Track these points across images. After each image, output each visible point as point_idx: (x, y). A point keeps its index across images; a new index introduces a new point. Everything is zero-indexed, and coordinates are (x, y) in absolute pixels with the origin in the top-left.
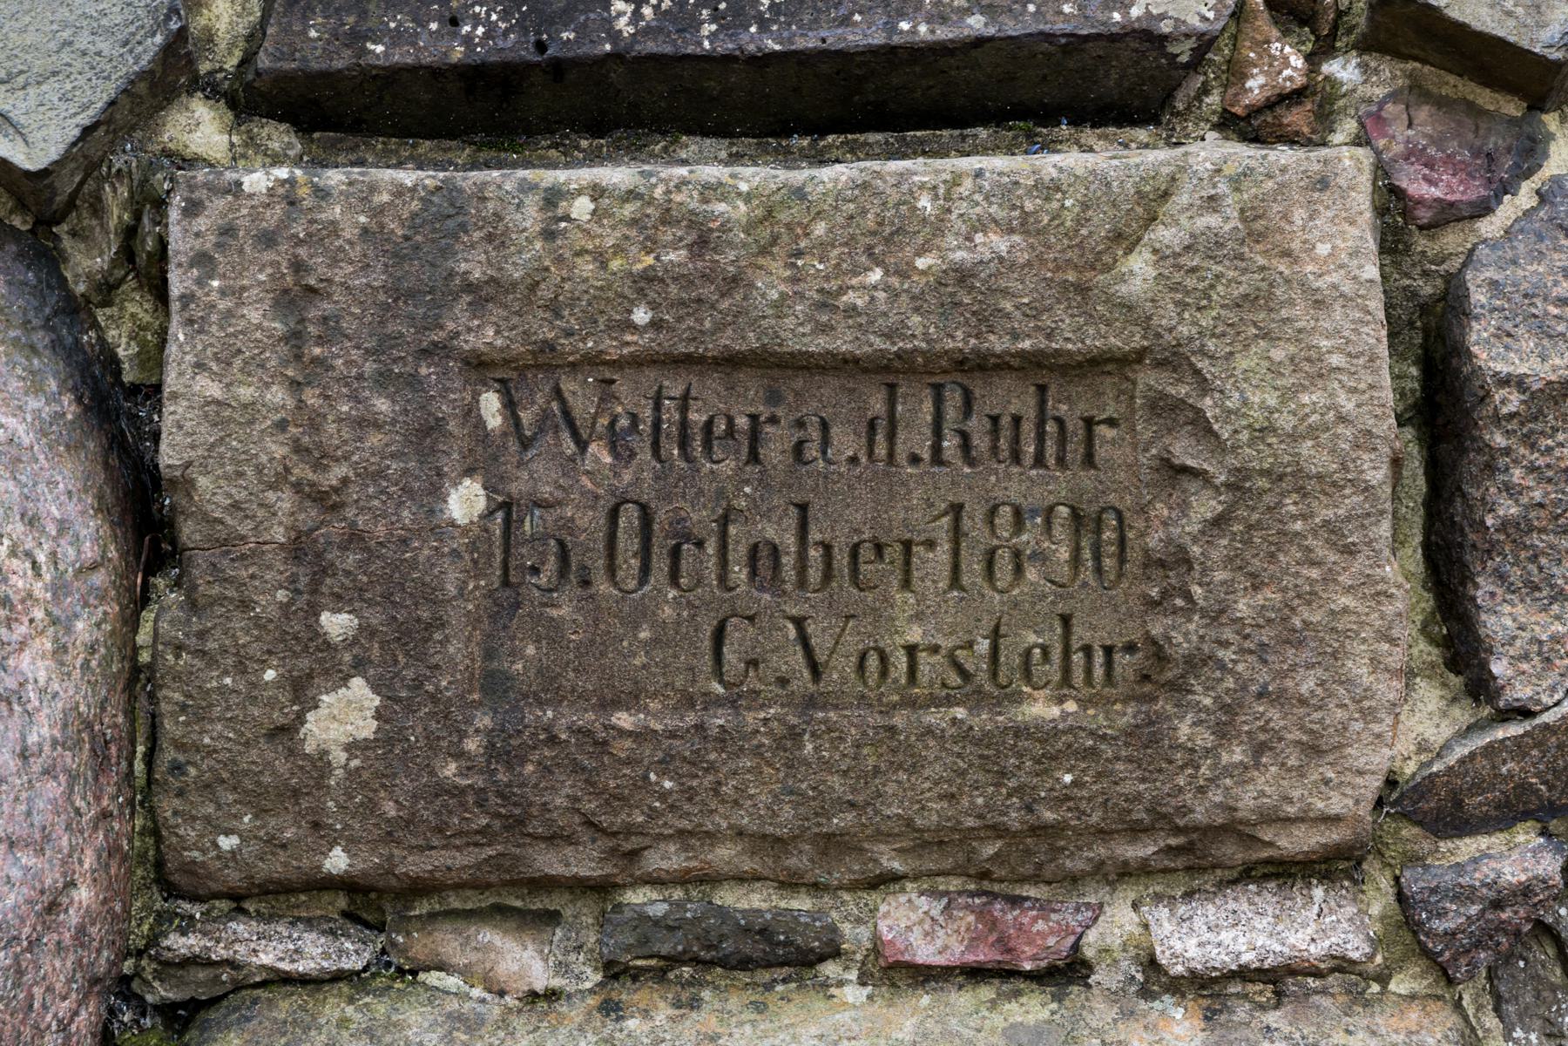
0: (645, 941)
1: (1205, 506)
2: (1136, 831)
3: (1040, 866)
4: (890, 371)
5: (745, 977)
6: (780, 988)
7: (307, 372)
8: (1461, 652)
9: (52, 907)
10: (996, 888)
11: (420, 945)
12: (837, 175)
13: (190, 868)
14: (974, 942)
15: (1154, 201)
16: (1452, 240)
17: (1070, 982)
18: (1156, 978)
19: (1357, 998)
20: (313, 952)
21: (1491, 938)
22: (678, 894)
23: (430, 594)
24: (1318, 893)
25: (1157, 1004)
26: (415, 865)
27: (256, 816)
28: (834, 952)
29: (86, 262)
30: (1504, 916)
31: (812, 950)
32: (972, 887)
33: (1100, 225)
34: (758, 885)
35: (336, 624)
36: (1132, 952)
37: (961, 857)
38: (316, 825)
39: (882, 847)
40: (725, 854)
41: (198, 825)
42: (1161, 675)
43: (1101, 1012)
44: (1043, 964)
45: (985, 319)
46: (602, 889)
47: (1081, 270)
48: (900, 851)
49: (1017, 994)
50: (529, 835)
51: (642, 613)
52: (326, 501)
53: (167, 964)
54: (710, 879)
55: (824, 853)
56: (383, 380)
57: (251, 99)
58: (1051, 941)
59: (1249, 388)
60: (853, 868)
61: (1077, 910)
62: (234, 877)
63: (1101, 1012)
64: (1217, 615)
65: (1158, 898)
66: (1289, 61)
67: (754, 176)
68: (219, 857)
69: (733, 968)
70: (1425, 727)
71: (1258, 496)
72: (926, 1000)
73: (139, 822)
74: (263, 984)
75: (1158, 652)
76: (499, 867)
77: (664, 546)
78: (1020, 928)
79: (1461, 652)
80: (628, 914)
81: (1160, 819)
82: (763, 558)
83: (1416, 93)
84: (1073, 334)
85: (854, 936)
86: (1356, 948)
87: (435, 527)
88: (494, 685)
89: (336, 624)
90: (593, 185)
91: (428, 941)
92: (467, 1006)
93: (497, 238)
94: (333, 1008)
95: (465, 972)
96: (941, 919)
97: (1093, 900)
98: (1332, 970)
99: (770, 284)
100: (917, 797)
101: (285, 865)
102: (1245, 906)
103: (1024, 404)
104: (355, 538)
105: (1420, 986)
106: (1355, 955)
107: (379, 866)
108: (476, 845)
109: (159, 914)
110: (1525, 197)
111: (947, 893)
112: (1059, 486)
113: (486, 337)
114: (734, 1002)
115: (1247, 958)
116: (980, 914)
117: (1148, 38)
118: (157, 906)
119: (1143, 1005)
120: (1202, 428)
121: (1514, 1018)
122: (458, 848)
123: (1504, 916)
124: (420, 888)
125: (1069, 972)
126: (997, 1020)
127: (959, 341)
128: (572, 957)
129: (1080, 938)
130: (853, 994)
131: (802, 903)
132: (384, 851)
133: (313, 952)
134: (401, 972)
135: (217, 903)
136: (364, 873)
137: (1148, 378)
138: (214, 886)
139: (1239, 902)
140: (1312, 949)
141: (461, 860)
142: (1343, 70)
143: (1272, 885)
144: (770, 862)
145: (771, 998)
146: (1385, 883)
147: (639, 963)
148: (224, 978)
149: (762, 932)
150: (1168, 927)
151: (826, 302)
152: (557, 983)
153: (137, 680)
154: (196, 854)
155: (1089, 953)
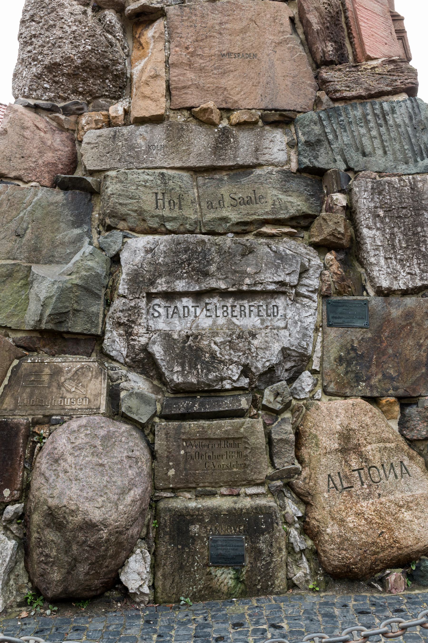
1: (249, 451)
2: (244, 481)
4: (220, 439)
7: (168, 441)
8: (273, 464)
11: (178, 494)
12: (215, 422)
15: (243, 424)
16: (270, 427)
18: (246, 495)
19: (265, 497)
20: (169, 495)
23: (179, 461)
26: (178, 486)
28: (217, 494)
29: (147, 432)
33: (239, 426)
35: (171, 464)
40: (207, 484)
42: (246, 466)
43: (241, 498)
45: (229, 434)
46: (195, 488)
47: (237, 430)
51: (199, 462)
52: (170, 452)
54: (205, 487)
56: (175, 441)
57: (163, 417)
59: (252, 440)
60: (218, 485)
63: (241, 498)
64: (250, 461)
66: (255, 411)
67: (207, 422)
70: (270, 471)
71: (253, 450)
75: (245, 464)
77: (200, 456)
79: (273, 464)
81: (246, 480)
82: (209, 457)
83: (266, 414)
84: (237, 436)
85: (218, 492)
87: (180, 454)
88: (185, 469)
89: (171, 464)
90: (193, 424)
93: (185, 428)
94: (171, 500)
99: (209, 432)
100: (224, 478)
103: (232, 442)
104: (172, 456)
110: (277, 423)
112: (235, 450)
113: (184, 437)
117: (242, 410)
120: (248, 444)
124: (179, 488)
125: (238, 495)
127: (226, 436)
133: (169, 495)
137: (243, 439)
139: (254, 488)
141: (182, 485)
142: (260, 412)
151: (214, 433)
153: (153, 470)
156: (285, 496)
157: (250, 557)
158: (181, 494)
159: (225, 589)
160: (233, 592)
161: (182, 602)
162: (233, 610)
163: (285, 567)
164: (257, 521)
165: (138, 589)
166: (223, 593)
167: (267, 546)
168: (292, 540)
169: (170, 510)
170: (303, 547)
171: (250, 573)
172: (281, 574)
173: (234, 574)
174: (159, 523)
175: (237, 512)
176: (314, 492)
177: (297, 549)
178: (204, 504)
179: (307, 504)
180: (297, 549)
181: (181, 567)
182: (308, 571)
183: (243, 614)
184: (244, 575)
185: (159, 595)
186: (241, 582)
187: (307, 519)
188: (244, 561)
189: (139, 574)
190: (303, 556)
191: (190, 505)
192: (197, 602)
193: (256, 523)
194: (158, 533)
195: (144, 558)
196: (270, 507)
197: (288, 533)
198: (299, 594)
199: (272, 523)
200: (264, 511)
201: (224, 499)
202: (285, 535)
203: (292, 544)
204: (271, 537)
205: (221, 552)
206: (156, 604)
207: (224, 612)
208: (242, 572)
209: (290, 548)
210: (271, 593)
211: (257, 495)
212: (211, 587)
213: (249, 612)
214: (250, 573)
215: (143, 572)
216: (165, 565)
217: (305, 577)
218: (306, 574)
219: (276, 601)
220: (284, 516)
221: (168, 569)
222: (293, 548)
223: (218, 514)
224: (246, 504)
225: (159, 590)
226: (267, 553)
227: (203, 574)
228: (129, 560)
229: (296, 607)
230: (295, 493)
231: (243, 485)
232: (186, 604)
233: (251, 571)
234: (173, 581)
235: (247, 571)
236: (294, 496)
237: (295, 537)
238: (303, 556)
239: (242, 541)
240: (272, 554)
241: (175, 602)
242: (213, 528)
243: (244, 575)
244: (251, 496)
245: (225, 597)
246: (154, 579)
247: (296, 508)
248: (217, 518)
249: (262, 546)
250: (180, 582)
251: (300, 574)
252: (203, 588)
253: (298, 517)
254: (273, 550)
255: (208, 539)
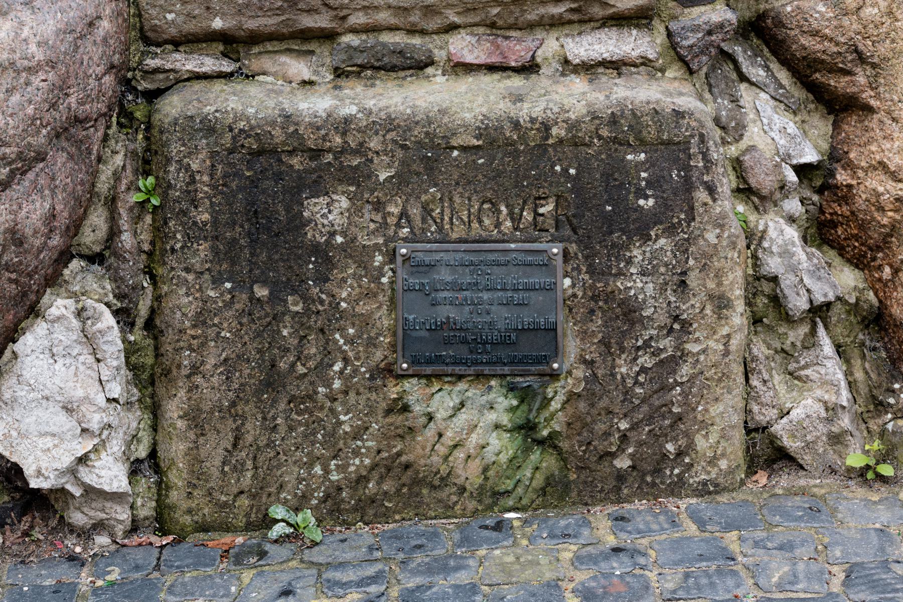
0: (350, 58)
3: (517, 19)
5: (394, 75)
6: (409, 79)
9: (91, 24)
10: (499, 32)
11: (255, 64)
13: (154, 29)
14: (490, 54)
17: (531, 73)
18: (568, 67)
21: (707, 49)
22: (364, 37)
24: (634, 32)
25: (568, 78)
26: (251, 24)
27: (182, 5)
28: (431, 63)
30: (713, 38)
31: (422, 61)
32: (489, 32)
34: (398, 32)
36: (557, 58)
37: (483, 16)
38: (208, 8)
39: (450, 11)
40: (383, 17)
41: (157, 9)
44: (520, 64)
46: (328, 36)
48: (458, 13)
49: (509, 77)
50: (299, 10)
53: (146, 72)
55: (425, 15)
58: (523, 54)
60: (433, 24)
61: (533, 40)
62: (173, 31)
65: (567, 35)
68: (167, 23)
69: (389, 71)
72: (471, 79)
73: (132, 11)
74: (188, 80)
76: (287, 25)
78: (509, 48)
80: (343, 45)
85: (440, 55)
86: (651, 55)
91: (259, 62)
92: (275, 87)
94: (218, 86)
95: (275, 75)
96: (476, 45)
97: (539, 37)
98: (643, 64)
101: (195, 26)
102: (604, 36)
105: (678, 74)
106: (651, 57)
107: (236, 25)
108: (277, 15)
109: (142, 53)
111: (478, 34)
114: (389, 84)
115: (605, 56)
116: (492, 43)
118: (142, 49)
119: (562, 79)
121: (717, 94)
122: (269, 16)
123: (713, 38)
124: (255, 39)
125: (530, 68)
126: (501, 85)
128: (320, 69)
129: (535, 53)
130: (440, 79)
131: (416, 41)
132: (238, 19)
133: (209, 64)
134: (247, 77)
135: (167, 46)
136: (229, 29)
138: (165, 36)
139: (603, 34)
140: (633, 53)
141: (267, 23)
143: (615, 28)
144: (402, 19)
145: (405, 83)
146: (662, 29)
147: (349, 69)
148: (171, 77)
149: (400, 52)
150: (571, 45)
152: (314, 78)
154: (156, 21)
155: (539, 60)
156: (743, 78)
157: (584, 335)
158: (266, 63)
159: (470, 474)
160: (509, 484)
161: (279, 529)
162: (504, 568)
163: (741, 379)
164: (616, 180)
165: (72, 472)
166: (463, 489)
167: (663, 289)
168: (773, 265)
169: (209, 128)
170: (822, 293)
171: (582, 406)
172: (723, 411)
173: (512, 410)
174: (163, 187)
175: (523, 138)
176: (884, 49)
177: (798, 303)
178: (370, 104)
179: (840, 107)
180: (798, 303)
181: (272, 381)
182: (845, 397)
183: (554, 585)
184: (555, 417)
185: (174, 496)
186: (541, 442)
187: (842, 177)
188: (556, 352)
189: (68, 409)
190: (821, 331)
191: (303, 106)
192: (348, 525)
193: (610, 193)
194: (159, 232)
195: (89, 340)
196: (679, 114)
197: (754, 239)
198: (803, 492)
199: (688, 186)
200: (651, 133)
201: (466, 84)
202: (742, 243)
203: (775, 279)
204: (683, 248)
205: (453, 313)
206: (164, 533)
207: (463, 577)
208: (546, 402)
209: (762, 301)
210: (677, 488)
211: (616, 66)
212: (407, 466)
213: (582, 576)
214: (582, 406)
215: (87, 399)
216: (195, 370)
217: (829, 420)
218: (832, 410)
219: (701, 524)
220: (738, 165)
221: (212, 390)
222: (777, 301)
223: (434, 147)
224: (568, 102)
225: (177, 478)
226: (663, 319)
227: (372, 411)
228: (18, 347)
229: (804, 552)
230: (787, 62)
231: (555, 23)
232: (295, 536)
233: (590, 396)
234: (237, 439)
235: (572, 397)
236: (783, 76)
237: (786, 253)
238: (821, 331)
239: (547, 265)
240: (686, 326)
241: (249, 527)
242: (415, 212)
243: (555, 417)
244: (588, 68)
245: (472, 505)
246: (155, 428)
247: (792, 128)
248: (430, 166)
249: (638, 286)
250: (270, 444)
251: (805, 407)
252: (374, 467)
253: (802, 170)
254: (690, 307)
255: (392, 256)
